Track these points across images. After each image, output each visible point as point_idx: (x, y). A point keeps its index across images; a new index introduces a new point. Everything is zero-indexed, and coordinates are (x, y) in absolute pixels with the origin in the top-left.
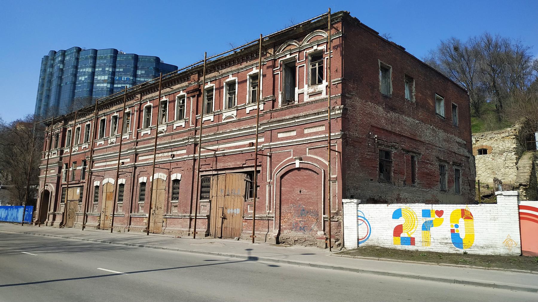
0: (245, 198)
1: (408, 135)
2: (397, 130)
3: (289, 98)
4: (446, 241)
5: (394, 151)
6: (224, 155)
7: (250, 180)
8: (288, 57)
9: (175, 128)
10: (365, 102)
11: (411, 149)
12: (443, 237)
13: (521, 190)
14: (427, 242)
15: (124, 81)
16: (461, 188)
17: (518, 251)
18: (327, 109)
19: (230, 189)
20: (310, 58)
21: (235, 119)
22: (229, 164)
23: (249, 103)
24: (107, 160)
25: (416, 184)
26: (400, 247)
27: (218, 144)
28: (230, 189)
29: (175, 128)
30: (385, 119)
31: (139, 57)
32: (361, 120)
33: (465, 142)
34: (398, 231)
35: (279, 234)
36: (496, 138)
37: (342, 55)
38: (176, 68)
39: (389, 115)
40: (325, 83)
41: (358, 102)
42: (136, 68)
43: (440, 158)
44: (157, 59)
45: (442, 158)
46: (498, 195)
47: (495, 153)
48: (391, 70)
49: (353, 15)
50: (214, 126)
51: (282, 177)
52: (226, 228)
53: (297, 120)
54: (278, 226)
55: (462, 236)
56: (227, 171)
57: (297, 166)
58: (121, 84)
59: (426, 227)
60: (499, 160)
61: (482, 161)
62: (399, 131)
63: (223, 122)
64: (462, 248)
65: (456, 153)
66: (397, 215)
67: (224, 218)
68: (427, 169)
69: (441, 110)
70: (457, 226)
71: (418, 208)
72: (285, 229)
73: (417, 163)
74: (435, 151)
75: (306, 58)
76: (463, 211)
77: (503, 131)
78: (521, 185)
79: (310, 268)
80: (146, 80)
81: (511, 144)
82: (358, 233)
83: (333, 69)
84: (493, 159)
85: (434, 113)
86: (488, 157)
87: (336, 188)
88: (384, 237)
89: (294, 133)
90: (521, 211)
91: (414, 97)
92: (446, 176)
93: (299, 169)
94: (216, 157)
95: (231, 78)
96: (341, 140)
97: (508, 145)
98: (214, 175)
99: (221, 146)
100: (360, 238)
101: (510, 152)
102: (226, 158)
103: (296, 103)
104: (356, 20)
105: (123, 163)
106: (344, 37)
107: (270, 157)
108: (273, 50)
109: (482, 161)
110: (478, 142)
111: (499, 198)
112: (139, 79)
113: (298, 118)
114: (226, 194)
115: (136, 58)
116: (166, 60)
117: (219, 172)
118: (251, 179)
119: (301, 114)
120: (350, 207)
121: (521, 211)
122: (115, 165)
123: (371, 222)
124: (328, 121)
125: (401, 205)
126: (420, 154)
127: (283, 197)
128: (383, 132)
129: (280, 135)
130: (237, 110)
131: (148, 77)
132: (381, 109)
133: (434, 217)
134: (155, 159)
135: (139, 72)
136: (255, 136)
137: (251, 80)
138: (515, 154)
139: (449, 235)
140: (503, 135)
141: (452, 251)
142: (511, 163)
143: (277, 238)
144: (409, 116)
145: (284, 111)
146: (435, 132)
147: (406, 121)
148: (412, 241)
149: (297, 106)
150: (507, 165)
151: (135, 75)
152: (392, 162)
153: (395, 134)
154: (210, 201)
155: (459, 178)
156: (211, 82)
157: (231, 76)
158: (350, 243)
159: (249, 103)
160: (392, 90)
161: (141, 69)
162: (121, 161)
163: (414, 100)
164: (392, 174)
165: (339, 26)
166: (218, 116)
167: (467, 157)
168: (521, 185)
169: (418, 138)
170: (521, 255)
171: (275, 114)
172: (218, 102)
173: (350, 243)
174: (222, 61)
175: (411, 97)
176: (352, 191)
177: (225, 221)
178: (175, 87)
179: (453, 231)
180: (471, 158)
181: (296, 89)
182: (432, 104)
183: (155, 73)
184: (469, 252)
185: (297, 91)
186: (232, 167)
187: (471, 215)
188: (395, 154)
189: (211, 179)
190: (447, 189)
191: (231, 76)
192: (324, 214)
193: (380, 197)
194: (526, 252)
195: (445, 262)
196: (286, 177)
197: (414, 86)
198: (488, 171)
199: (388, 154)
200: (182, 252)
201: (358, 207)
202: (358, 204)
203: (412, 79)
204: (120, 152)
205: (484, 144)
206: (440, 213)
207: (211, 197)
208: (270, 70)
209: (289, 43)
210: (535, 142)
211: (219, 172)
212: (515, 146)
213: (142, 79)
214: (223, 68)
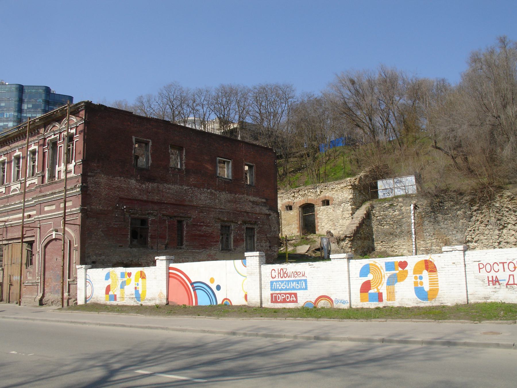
0: (27, 266)
1: (173, 201)
2: (156, 198)
3: (52, 176)
4: (132, 296)
5: (151, 218)
6: (12, 226)
7: (30, 249)
8: (53, 137)
9: (27, 185)
10: (112, 177)
11: (176, 214)
12: (131, 293)
13: (347, 242)
14: (122, 298)
15: (7, 118)
16: (256, 245)
17: (165, 302)
18: (64, 189)
19: (15, 258)
20: (66, 139)
21: (18, 192)
22: (15, 234)
23: (29, 177)
24: (9, 213)
25: (184, 246)
26: (109, 303)
27: (8, 215)
28: (15, 258)
29: (27, 185)
30: (138, 190)
31: (25, 88)
32: (106, 194)
33: (264, 200)
34: (366, 287)
35: (43, 296)
36: (336, 189)
37: (84, 140)
38: (71, 98)
39: (144, 186)
40: (74, 163)
41: (103, 179)
42: (21, 101)
43: (222, 218)
44: (47, 90)
45: (226, 219)
46: (158, 259)
47: (335, 204)
48: (150, 144)
49: (95, 102)
50: (5, 198)
51: (46, 246)
52: (13, 293)
53: (55, 196)
54: (42, 290)
55: (140, 292)
56: (15, 241)
57: (54, 237)
58: (4, 121)
59: (122, 287)
60: (338, 211)
61: (325, 212)
62: (159, 200)
63: (11, 194)
64: (139, 301)
65: (248, 213)
66: (107, 277)
67: (11, 285)
68: (200, 231)
69: (226, 172)
70: (138, 284)
71: (120, 270)
72: (47, 292)
73: (185, 226)
74: (213, 213)
75: (64, 139)
76: (426, 262)
77: (343, 181)
78: (346, 237)
79: (98, 327)
80: (34, 115)
81: (348, 194)
82: (261, 293)
83: (78, 152)
84: (333, 211)
85: (214, 176)
86: (329, 209)
87: (76, 255)
88: (99, 296)
89: (54, 207)
90: (171, 271)
91: (184, 165)
92: (232, 236)
93: (56, 239)
94: (6, 227)
95: (18, 153)
96: (80, 214)
97: (346, 195)
98: (5, 245)
99: (11, 217)
100: (88, 297)
101: (347, 202)
102: (13, 228)
103: (56, 179)
104: (101, 106)
105: (30, 216)
106: (86, 123)
107: (40, 228)
108: (43, 129)
109: (325, 212)
110: (322, 193)
111: (158, 262)
112: (25, 115)
113: (55, 193)
114: (13, 262)
115: (21, 89)
116: (56, 89)
117: (10, 242)
118: (31, 248)
119: (57, 191)
120: (81, 271)
121: (171, 271)
122: (19, 219)
123: (95, 282)
124: (64, 199)
125: (110, 269)
126: (190, 218)
127: (46, 265)
128: (136, 202)
129: (47, 209)
130: (21, 183)
131: (36, 112)
132: (133, 181)
133: (126, 278)
134: (65, 210)
135: (25, 107)
136: (22, 211)
137: (32, 155)
138: (351, 205)
139: (133, 291)
140: (342, 185)
141: (135, 304)
142: (347, 214)
143: (41, 301)
144: (174, 183)
145: (48, 187)
146: (215, 195)
147: (169, 189)
148: (115, 297)
149: (56, 183)
150: (344, 216)
151: (20, 110)
152: (148, 228)
153: (153, 202)
154: (3, 270)
155: (254, 236)
156: (4, 155)
157: (17, 150)
158: (81, 301)
159: (29, 177)
160: (150, 162)
161: (28, 103)
162: (26, 214)
163: (184, 167)
164: (149, 239)
165: (82, 113)
166: (8, 188)
167: (266, 214)
168: (346, 237)
169: (187, 203)
170: (167, 304)
171: (43, 189)
172: (8, 176)
173: (81, 301)
174: (10, 136)
175: (181, 165)
176: (94, 258)
177: (12, 287)
178: (13, 145)
179: (136, 288)
180: (273, 215)
181: (57, 166)
182: (210, 168)
183: (45, 107)
184: (143, 304)
185: (57, 169)
186: (16, 237)
187: (435, 267)
188: (153, 221)
189: (4, 248)
190: (232, 248)
191: (17, 150)
192: (69, 278)
193: (132, 261)
194: (172, 302)
195: (257, 317)
196: (49, 246)
197: (184, 154)
198: (330, 222)
199: (144, 222)
200: (105, 327)
201: (464, 255)
202: (86, 269)
203: (182, 148)
204: (25, 202)
205: (327, 195)
206: (129, 274)
207: (3, 265)
208: (42, 148)
209: (54, 124)
210: (377, 191)
211: (10, 242)
212: (351, 196)
213: (29, 115)
214: (13, 143)
